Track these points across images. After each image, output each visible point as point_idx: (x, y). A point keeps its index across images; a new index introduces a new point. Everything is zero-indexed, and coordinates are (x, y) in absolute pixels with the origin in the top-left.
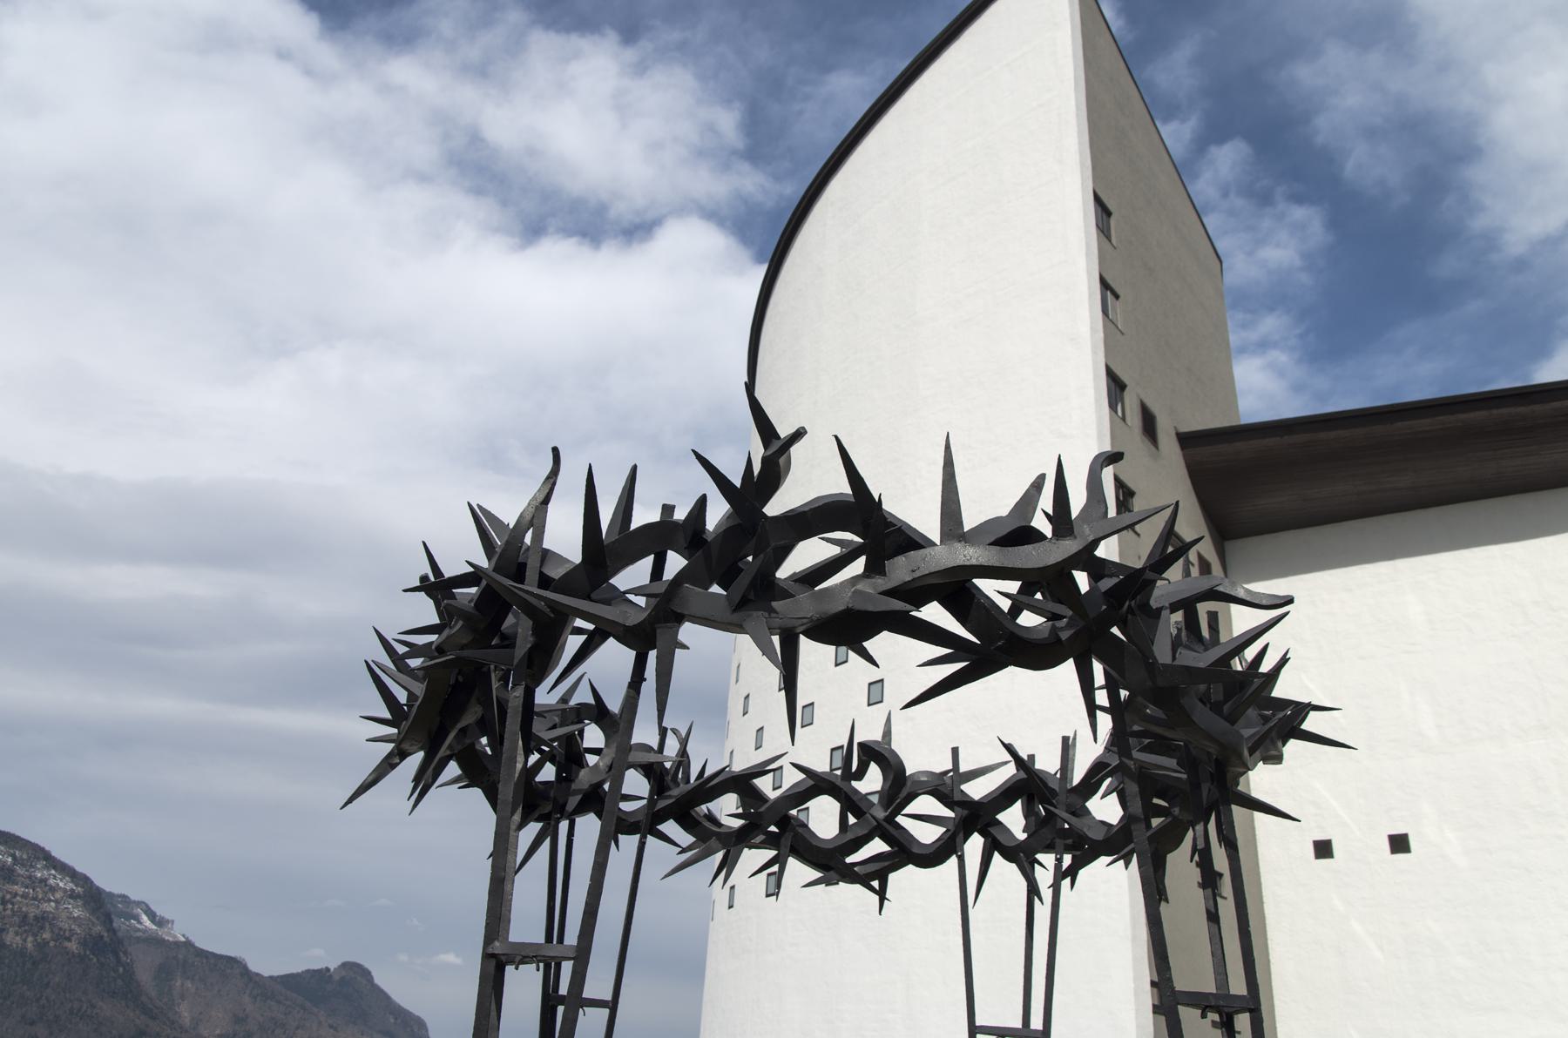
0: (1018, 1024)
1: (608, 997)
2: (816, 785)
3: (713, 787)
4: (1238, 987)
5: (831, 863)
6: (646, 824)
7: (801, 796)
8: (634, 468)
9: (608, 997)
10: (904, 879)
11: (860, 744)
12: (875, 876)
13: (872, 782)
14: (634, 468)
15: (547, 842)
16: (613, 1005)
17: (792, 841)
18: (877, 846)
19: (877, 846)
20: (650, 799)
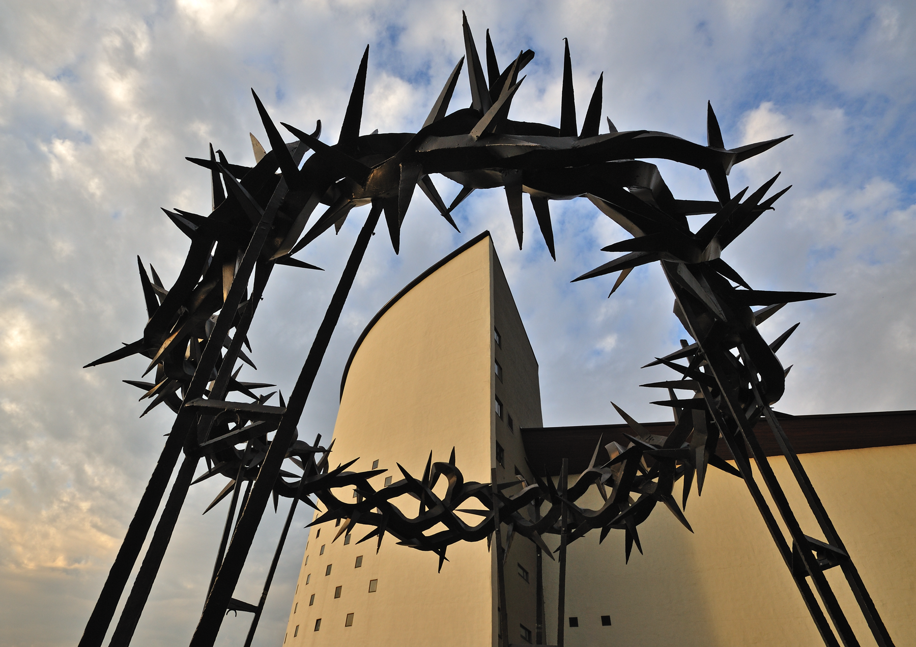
0: (769, 342)
1: (256, 604)
2: (409, 486)
3: (341, 478)
4: (208, 498)
5: (409, 533)
6: (299, 492)
7: (395, 490)
8: (188, 159)
9: (256, 604)
10: (457, 549)
11: (436, 464)
12: (439, 545)
13: (441, 489)
14: (188, 159)
15: (232, 493)
16: (257, 610)
17: (391, 522)
18: (440, 527)
19: (440, 527)
20: (303, 478)
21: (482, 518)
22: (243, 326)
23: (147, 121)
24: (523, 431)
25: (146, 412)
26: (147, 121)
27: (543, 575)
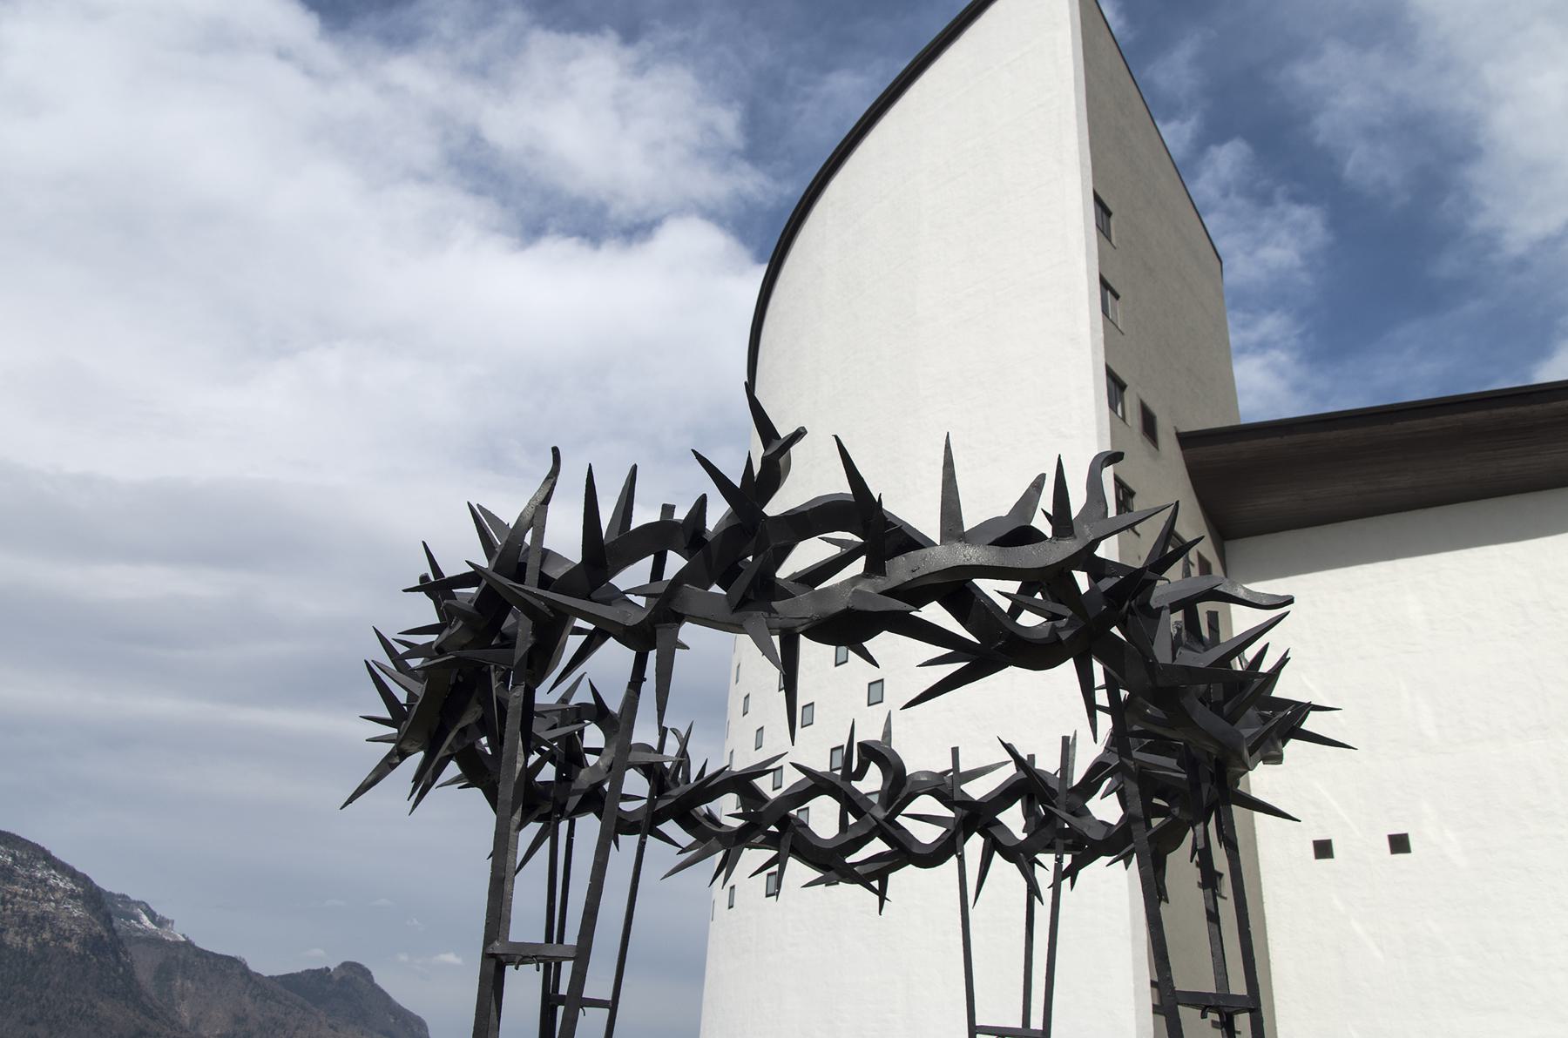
1: (608, 997)
2: (816, 785)
3: (713, 787)
5: (831, 863)
6: (646, 824)
7: (800, 796)
8: (635, 468)
9: (608, 997)
11: (860, 744)
13: (872, 782)
14: (635, 468)
16: (613, 1005)
18: (877, 846)
19: (877, 846)
20: (651, 799)
21: (941, 830)
22: (402, 759)
23: (1304, 74)
24: (1187, 440)
25: (350, 801)
26: (1304, 74)
27: (1307, 531)
